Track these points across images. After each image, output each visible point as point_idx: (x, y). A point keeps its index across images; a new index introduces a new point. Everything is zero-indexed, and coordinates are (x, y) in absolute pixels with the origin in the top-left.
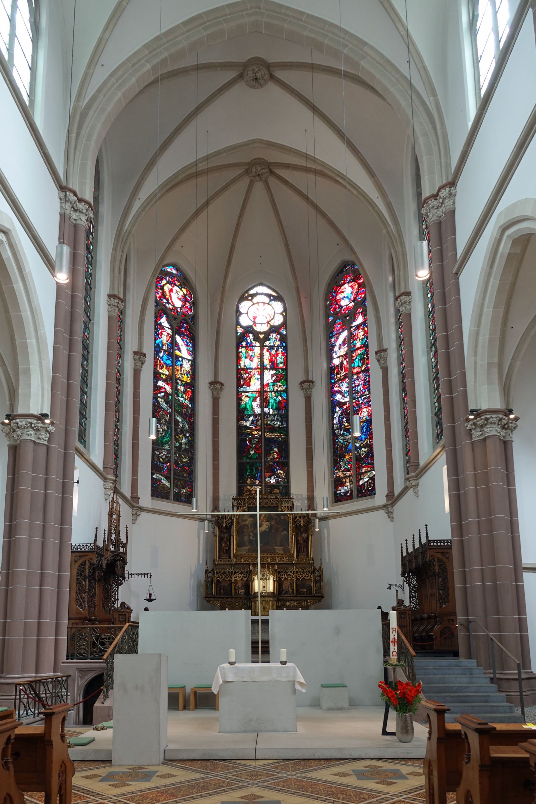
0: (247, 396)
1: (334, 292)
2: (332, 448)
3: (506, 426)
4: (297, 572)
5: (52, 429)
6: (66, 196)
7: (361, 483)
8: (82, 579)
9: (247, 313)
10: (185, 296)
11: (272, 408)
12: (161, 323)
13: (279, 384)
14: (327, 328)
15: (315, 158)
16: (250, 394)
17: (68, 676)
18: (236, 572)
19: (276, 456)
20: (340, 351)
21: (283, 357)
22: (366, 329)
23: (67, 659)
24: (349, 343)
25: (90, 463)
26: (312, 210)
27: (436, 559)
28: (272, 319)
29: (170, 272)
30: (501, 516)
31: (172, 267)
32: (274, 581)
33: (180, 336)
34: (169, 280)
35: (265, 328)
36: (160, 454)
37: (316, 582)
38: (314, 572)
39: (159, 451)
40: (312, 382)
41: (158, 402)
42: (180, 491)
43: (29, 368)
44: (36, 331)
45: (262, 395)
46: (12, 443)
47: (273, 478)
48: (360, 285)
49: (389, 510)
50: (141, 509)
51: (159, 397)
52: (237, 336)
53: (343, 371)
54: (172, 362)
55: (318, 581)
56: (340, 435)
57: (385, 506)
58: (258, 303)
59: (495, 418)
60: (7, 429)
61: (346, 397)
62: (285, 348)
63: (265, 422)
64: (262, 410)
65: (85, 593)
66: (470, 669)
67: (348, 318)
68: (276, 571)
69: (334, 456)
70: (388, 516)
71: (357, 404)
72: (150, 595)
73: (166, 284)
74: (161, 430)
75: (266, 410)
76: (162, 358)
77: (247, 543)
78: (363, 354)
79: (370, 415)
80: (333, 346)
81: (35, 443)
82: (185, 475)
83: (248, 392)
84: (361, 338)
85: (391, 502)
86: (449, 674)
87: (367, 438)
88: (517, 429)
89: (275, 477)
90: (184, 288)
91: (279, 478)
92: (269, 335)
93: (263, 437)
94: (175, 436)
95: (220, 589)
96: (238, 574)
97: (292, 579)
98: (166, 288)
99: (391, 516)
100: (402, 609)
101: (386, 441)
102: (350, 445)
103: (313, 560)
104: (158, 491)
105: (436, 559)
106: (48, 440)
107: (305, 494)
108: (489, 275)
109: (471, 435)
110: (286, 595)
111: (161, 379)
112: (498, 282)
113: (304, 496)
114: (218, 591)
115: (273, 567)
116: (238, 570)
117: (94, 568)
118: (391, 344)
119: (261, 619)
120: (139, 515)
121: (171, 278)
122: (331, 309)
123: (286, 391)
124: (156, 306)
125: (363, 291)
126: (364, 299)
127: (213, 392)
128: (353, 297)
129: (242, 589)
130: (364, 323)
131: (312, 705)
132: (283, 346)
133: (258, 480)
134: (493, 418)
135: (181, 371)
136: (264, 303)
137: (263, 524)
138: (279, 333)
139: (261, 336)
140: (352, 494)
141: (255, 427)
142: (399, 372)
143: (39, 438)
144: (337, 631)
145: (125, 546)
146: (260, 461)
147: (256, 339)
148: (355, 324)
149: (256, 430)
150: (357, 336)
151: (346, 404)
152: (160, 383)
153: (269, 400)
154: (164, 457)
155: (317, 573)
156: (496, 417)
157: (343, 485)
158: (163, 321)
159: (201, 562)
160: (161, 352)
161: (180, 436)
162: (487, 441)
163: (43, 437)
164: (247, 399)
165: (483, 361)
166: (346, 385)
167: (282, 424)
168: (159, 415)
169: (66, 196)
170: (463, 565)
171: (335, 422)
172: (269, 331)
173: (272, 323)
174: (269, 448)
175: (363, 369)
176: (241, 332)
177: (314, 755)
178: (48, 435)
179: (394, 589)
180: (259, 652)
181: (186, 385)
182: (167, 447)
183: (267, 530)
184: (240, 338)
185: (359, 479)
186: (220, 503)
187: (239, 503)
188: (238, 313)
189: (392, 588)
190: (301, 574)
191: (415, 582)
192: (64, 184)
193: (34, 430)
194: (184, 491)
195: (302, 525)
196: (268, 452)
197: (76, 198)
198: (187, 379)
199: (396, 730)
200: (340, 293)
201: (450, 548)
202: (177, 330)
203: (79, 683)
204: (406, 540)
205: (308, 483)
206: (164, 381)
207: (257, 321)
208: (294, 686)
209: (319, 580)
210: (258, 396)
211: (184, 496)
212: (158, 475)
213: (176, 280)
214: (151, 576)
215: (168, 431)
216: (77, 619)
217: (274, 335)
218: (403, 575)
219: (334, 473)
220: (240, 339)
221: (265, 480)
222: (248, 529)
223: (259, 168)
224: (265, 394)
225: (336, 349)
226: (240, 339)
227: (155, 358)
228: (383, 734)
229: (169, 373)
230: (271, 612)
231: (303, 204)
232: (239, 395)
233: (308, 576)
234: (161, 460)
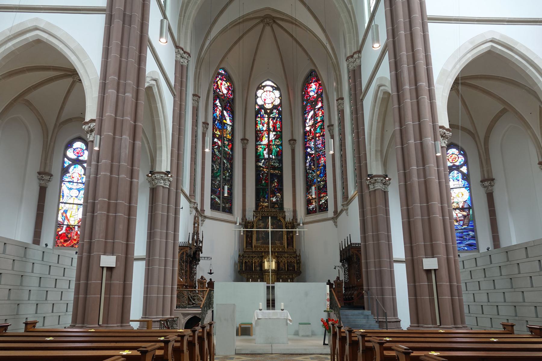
0: (261, 147)
1: (307, 87)
2: (306, 181)
3: (385, 183)
4: (287, 257)
5: (171, 179)
6: (178, 51)
7: (321, 203)
8: (182, 262)
9: (261, 97)
10: (228, 86)
11: (274, 155)
12: (216, 104)
13: (278, 140)
14: (303, 108)
15: (296, 19)
16: (262, 146)
17: (178, 318)
18: (255, 257)
19: (276, 185)
20: (309, 123)
21: (280, 124)
22: (323, 110)
23: (177, 308)
24: (314, 118)
25: (185, 194)
26: (294, 43)
27: (355, 254)
28: (274, 101)
29: (221, 73)
30: (383, 233)
31: (222, 70)
32: (275, 262)
33: (226, 111)
34: (220, 78)
35: (270, 106)
36: (215, 183)
38: (296, 257)
39: (214, 181)
40: (295, 140)
41: (214, 152)
42: (225, 206)
43: (162, 147)
44: (165, 127)
45: (269, 147)
46: (152, 186)
48: (320, 84)
49: (335, 221)
50: (206, 217)
51: (215, 148)
52: (255, 111)
53: (311, 135)
54: (222, 127)
56: (310, 173)
57: (332, 219)
58: (267, 91)
59: (379, 179)
60: (149, 179)
61: (313, 151)
62: (281, 119)
63: (271, 164)
64: (269, 156)
65: (183, 270)
66: (368, 316)
67: (313, 103)
68: (276, 256)
69: (307, 186)
70: (335, 224)
71: (318, 155)
72: (211, 270)
73: (219, 80)
74: (216, 168)
75: (271, 156)
76: (216, 124)
77: (261, 239)
78: (321, 126)
79: (325, 162)
80: (306, 119)
81: (163, 187)
83: (261, 145)
84: (320, 116)
85: (336, 216)
86: (358, 318)
87: (324, 176)
88: (391, 184)
89: (275, 198)
90: (228, 82)
92: (273, 111)
93: (269, 173)
94: (223, 172)
95: (247, 267)
98: (219, 83)
99: (336, 224)
100: (339, 282)
101: (333, 179)
102: (315, 180)
103: (296, 250)
104: (214, 206)
105: (355, 254)
106: (169, 185)
107: (292, 209)
108: (374, 106)
109: (369, 188)
110: (281, 272)
111: (216, 137)
112: (378, 110)
113: (291, 210)
114: (246, 268)
115: (275, 254)
116: (256, 255)
117: (188, 256)
118: (336, 123)
119: (271, 286)
121: (222, 77)
122: (305, 97)
123: (281, 145)
124: (214, 94)
125: (321, 88)
126: (322, 93)
127: (243, 145)
128: (316, 91)
129: (258, 267)
130: (322, 107)
131: (295, 335)
132: (280, 117)
133: (267, 199)
134: (378, 180)
135: (226, 132)
136: (270, 91)
138: (278, 110)
139: (268, 111)
140: (316, 209)
141: (265, 166)
142: (339, 139)
143: (165, 184)
144: (306, 294)
145: (202, 242)
146: (267, 187)
147: (266, 113)
148: (317, 107)
149: (266, 168)
150: (318, 115)
151: (313, 155)
152: (216, 140)
153: (272, 150)
154: (217, 185)
155: (298, 258)
156: (380, 179)
157: (311, 204)
158: (217, 102)
159: (236, 249)
160: (216, 121)
161: (226, 172)
162: (376, 191)
163: (167, 183)
164: (261, 149)
165: (373, 149)
166: (313, 143)
167: (279, 165)
168: (215, 159)
169: (178, 51)
170: (366, 259)
171: (307, 165)
172: (273, 109)
173: (274, 103)
174: (272, 180)
175: (321, 134)
176: (258, 108)
177: (295, 352)
178: (169, 183)
179: (337, 268)
180: (270, 306)
181: (229, 140)
182: (219, 179)
184: (257, 112)
185: (320, 201)
186: (246, 213)
187: (257, 214)
188: (256, 97)
191: (347, 266)
192: (178, 45)
193: (163, 180)
196: (272, 182)
197: (183, 52)
198: (229, 137)
199: (328, 343)
200: (309, 88)
201: (360, 248)
202: (224, 108)
203: (183, 322)
204: (350, 235)
205: (293, 202)
206: (218, 138)
207: (266, 102)
208: (287, 321)
209: (299, 263)
210: (267, 148)
211: (227, 209)
212: (214, 196)
213: (224, 77)
214: (211, 259)
215: (219, 168)
216: (180, 285)
217: (275, 111)
218: (341, 261)
219: (307, 196)
220: (258, 112)
223: (268, 20)
224: (271, 146)
225: (308, 121)
226: (258, 112)
227: (213, 125)
228: (324, 345)
229: (220, 133)
230: (275, 283)
231: (290, 39)
232: (256, 146)
233: (293, 260)
234: (216, 186)
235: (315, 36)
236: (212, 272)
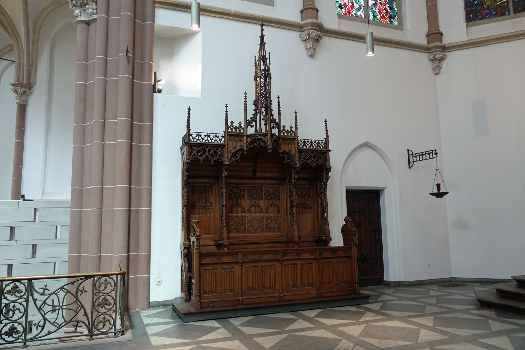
50: (445, 49)
72: (438, 186)
120: (15, 93)
214: (436, 154)
236: (442, 191)
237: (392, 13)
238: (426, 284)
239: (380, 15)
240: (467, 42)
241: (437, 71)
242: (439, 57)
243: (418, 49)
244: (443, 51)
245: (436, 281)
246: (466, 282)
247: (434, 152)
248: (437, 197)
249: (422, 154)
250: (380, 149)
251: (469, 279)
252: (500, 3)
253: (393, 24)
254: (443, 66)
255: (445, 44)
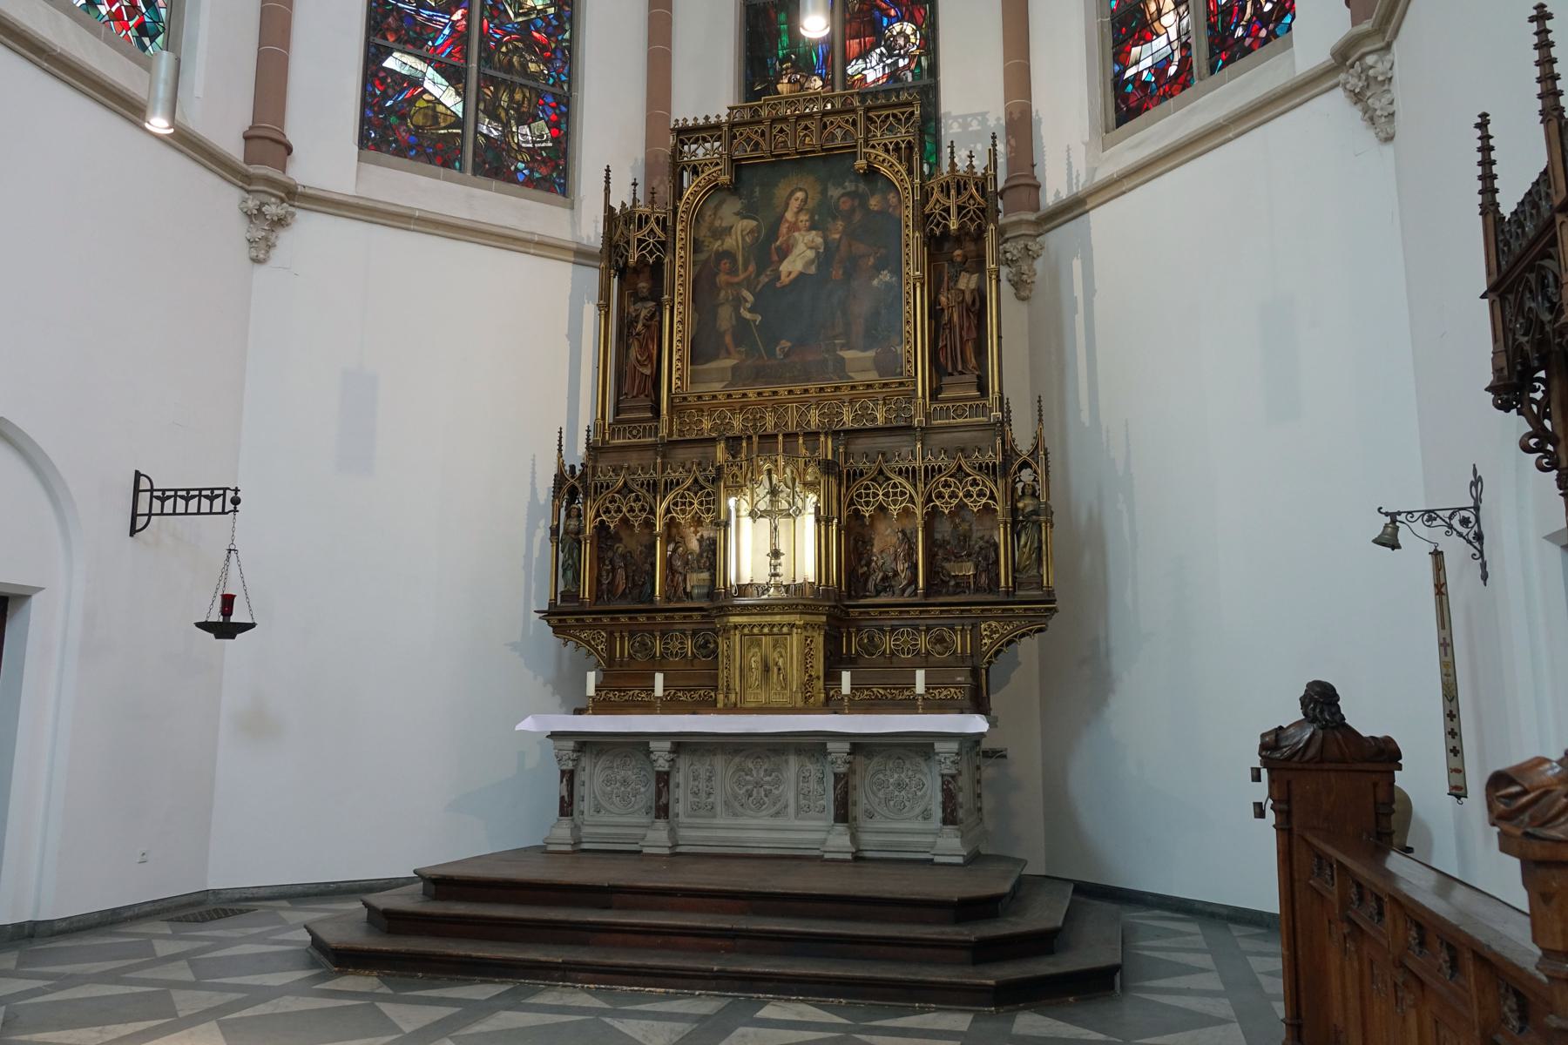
18: (671, 485)
37: (1017, 523)
42: (507, 132)
47: (875, 57)
50: (291, 194)
55: (1027, 516)
72: (228, 602)
77: (728, 339)
82: (533, 67)
89: (882, 54)
91: (899, 55)
96: (678, 490)
97: (906, 509)
107: (996, 115)
133: (820, 76)
137: (796, 240)
140: (1185, 63)
183: (813, 270)
189: (1403, 535)
190: (946, 485)
194: (524, 135)
195: (953, 225)
205: (1007, 57)
211: (527, 157)
214: (236, 501)
221: (844, 71)
222: (733, 271)
233: (981, 494)
235: (1296, 965)
237: (150, 20)
238: (125, 920)
239: (111, 7)
240: (351, 200)
241: (260, 251)
242: (272, 215)
243: (218, 166)
244: (286, 199)
245: (159, 908)
246: (247, 899)
247: (230, 495)
248: (217, 637)
249: (212, 493)
250: (39, 449)
251: (256, 890)
252: (446, 131)
253: (147, 53)
254: (278, 243)
255: (297, 182)
